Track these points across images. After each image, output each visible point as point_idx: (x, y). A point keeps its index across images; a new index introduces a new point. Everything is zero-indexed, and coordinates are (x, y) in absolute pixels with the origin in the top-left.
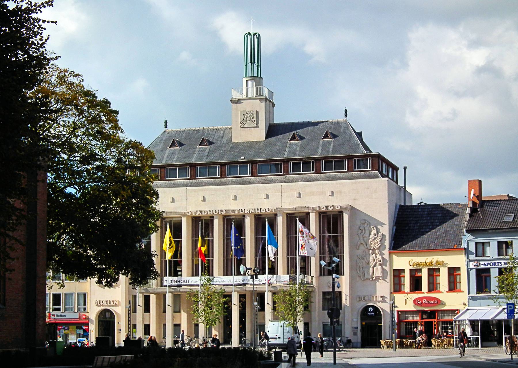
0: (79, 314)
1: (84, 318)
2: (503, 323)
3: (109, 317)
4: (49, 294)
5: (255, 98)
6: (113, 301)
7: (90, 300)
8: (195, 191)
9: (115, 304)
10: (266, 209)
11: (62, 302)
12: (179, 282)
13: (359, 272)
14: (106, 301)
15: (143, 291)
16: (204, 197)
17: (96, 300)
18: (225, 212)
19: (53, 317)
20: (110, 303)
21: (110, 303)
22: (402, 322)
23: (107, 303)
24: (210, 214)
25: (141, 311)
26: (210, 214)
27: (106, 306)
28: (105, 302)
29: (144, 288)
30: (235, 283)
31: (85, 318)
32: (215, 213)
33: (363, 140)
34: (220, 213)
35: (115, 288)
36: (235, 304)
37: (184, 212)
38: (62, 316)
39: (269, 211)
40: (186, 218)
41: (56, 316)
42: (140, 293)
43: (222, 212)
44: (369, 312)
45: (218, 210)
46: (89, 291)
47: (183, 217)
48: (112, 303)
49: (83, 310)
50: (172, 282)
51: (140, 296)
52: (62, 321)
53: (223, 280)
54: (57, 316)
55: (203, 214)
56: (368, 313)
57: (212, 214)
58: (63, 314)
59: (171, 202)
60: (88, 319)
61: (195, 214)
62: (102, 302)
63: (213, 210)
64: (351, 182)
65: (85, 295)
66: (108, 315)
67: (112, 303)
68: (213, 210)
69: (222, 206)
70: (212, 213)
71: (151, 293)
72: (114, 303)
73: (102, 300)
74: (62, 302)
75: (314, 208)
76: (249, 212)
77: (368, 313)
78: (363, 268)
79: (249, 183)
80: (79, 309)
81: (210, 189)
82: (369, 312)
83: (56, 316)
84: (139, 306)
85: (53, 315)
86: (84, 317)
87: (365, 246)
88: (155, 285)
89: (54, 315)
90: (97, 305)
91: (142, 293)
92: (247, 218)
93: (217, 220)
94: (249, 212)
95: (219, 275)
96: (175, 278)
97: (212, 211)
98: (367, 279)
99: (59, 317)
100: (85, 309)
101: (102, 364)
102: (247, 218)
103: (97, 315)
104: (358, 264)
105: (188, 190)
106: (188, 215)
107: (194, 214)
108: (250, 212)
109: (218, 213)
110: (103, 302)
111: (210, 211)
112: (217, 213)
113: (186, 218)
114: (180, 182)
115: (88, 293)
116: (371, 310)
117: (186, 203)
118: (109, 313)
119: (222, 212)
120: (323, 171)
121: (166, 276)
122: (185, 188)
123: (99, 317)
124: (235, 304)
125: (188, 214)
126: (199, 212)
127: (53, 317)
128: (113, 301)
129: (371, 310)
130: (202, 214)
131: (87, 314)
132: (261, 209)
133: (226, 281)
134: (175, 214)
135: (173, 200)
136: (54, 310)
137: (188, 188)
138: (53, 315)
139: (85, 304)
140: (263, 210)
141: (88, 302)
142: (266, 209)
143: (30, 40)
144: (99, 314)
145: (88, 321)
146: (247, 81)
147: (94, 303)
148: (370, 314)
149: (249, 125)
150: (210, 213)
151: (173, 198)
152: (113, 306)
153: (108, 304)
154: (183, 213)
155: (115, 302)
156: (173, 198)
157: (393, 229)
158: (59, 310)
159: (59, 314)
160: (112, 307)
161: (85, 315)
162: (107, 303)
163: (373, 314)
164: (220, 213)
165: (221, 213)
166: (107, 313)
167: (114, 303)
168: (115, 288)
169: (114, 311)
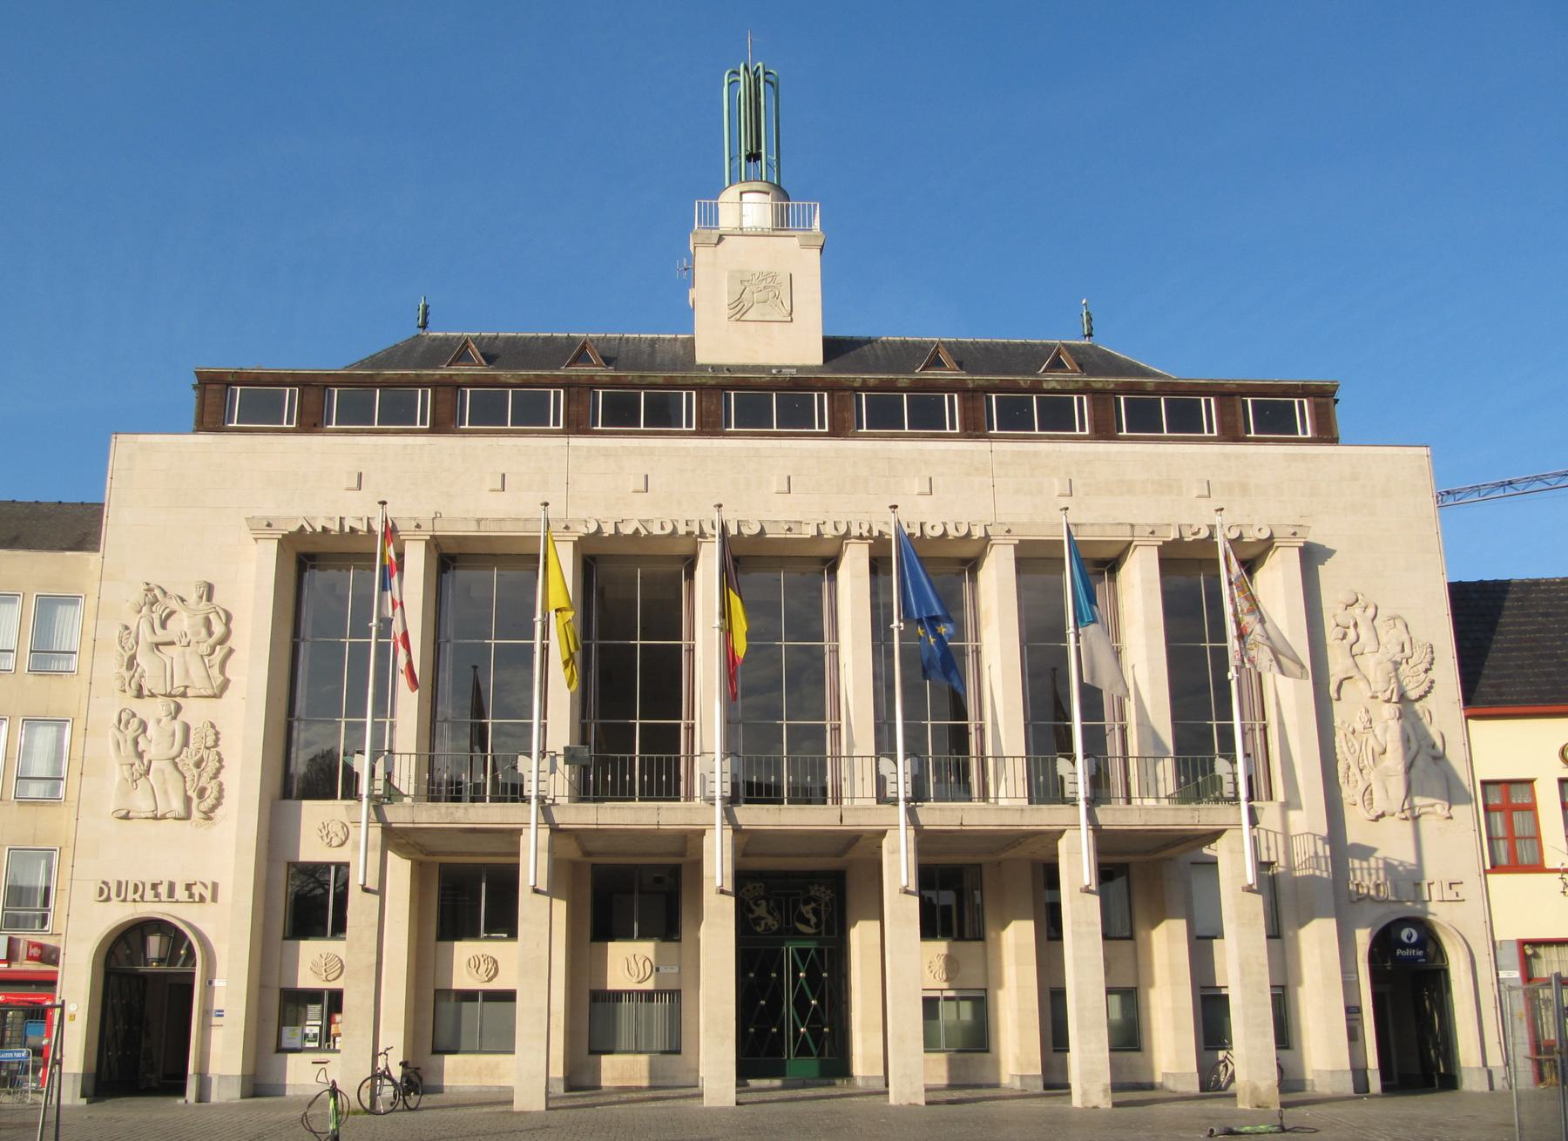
2: (484, 885)
5: (771, 233)
6: (188, 887)
10: (944, 524)
14: (154, 886)
20: (171, 893)
21: (171, 893)
22: (1087, 886)
28: (148, 887)
30: (436, 757)
33: (1265, 537)
44: (1404, 946)
56: (1399, 952)
62: (131, 889)
76: (870, 530)
82: (1404, 946)
94: (870, 530)
101: (417, 1105)
105: (576, 448)
110: (136, 891)
116: (1409, 938)
129: (1409, 938)
142: (944, 524)
143: (1400, 954)
144: (115, 936)
146: (741, 193)
148: (1407, 953)
149: (762, 314)
157: (1395, 860)
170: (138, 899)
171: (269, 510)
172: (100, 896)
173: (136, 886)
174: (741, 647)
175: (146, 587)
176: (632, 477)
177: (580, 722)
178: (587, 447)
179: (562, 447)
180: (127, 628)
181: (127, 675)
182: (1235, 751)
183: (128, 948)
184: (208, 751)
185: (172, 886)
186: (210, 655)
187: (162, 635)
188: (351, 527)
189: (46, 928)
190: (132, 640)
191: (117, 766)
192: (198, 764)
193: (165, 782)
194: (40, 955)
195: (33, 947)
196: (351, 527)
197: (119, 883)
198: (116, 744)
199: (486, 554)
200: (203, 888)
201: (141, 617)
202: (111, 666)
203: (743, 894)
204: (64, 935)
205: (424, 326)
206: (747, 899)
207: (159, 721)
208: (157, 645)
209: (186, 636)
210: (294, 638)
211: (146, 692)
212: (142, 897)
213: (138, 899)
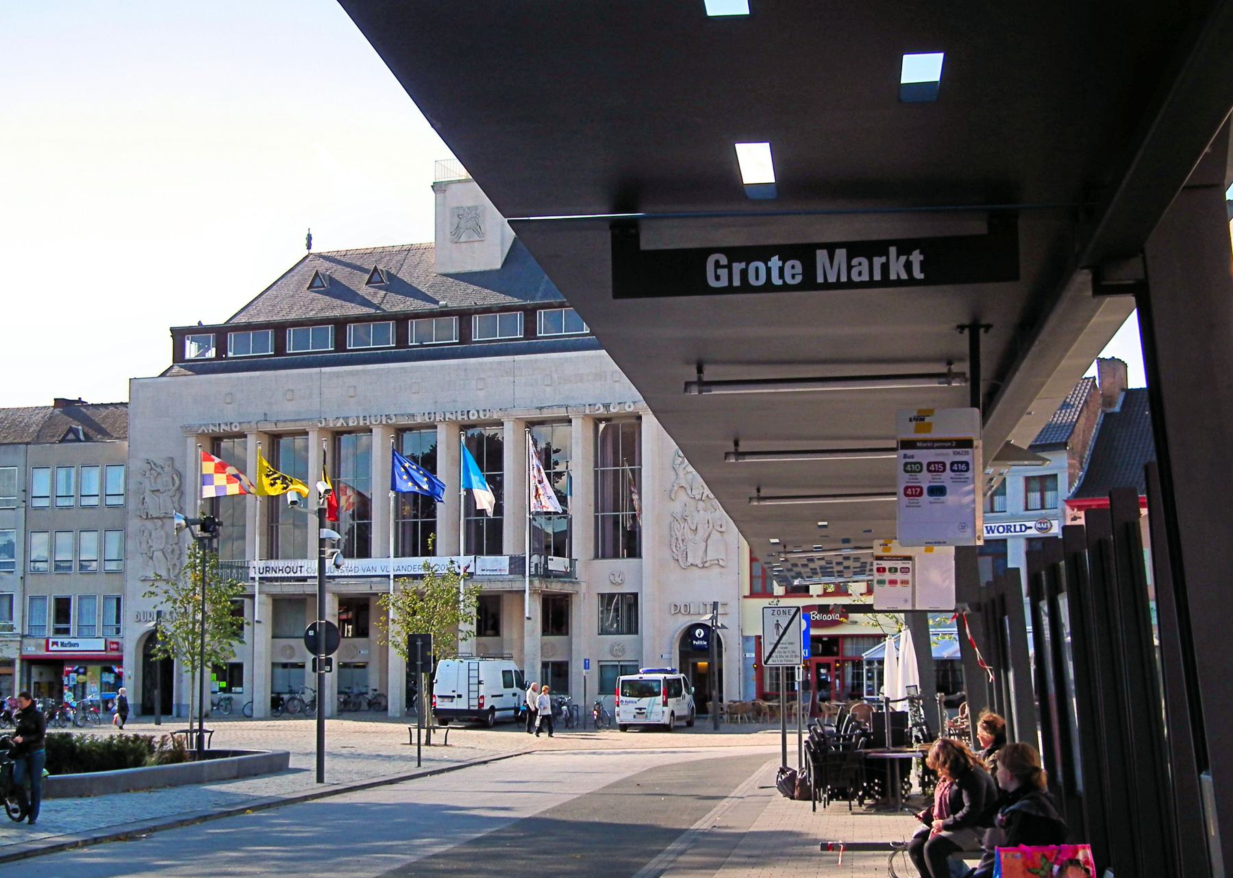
0: (106, 641)
13: (674, 550)
19: (55, 648)
34: (384, 422)
41: (60, 644)
54: (63, 644)
56: (694, 642)
58: (73, 641)
77: (694, 642)
78: (683, 540)
82: (697, 639)
83: (60, 644)
87: (689, 492)
98: (692, 564)
99: (66, 646)
104: (673, 533)
108: (447, 419)
127: (55, 648)
130: (348, 424)
136: (58, 631)
138: (54, 643)
158: (67, 631)
159: (66, 641)
163: (705, 643)
205: (309, 247)
208: (153, 491)
211: (149, 516)
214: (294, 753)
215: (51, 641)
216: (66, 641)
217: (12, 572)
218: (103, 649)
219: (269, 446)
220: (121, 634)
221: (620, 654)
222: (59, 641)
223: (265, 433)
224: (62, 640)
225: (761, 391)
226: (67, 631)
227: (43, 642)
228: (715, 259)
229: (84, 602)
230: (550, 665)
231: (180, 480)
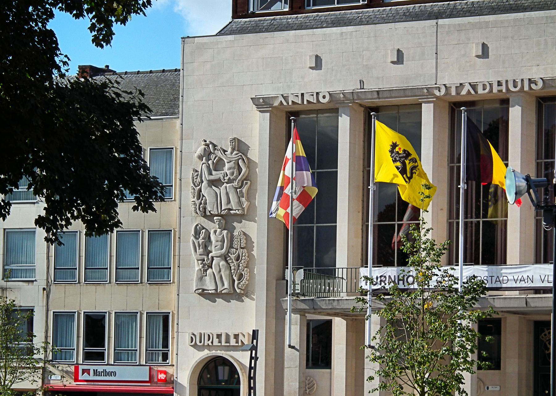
0: (150, 369)
1: (161, 380)
3: (226, 378)
4: (76, 315)
6: (236, 336)
7: (178, 332)
8: (460, 29)
9: (240, 344)
11: (109, 337)
12: (530, 281)
15: (303, 306)
16: (484, 46)
17: (191, 331)
18: (540, 84)
19: (86, 377)
20: (228, 341)
21: (228, 341)
23: (220, 342)
24: (500, 91)
25: (297, 363)
26: (500, 91)
27: (221, 347)
28: (215, 337)
29: (307, 298)
31: (165, 381)
32: (512, 88)
34: (526, 88)
35: (243, 301)
36: (293, 347)
37: (428, 89)
38: (106, 373)
39: (515, 87)
40: (432, 105)
41: (92, 372)
42: (295, 311)
43: (533, 86)
45: (522, 80)
46: (176, 309)
47: (425, 102)
48: (233, 342)
49: (160, 358)
50: (381, 281)
51: (293, 321)
52: (108, 388)
53: (525, 277)
54: (96, 373)
55: (480, 91)
57: (504, 91)
58: (109, 369)
59: (393, 62)
60: (172, 382)
61: (458, 93)
63: (507, 81)
64: (515, 20)
65: (166, 318)
66: (223, 373)
67: (233, 342)
68: (507, 81)
69: (535, 69)
70: (504, 89)
71: (336, 315)
72: (237, 342)
73: (208, 332)
74: (109, 337)
75: (267, 100)
79: (361, 23)
80: (150, 356)
81: (502, 22)
83: (92, 372)
84: (290, 346)
85: (84, 371)
86: (162, 376)
88: (344, 290)
89: (88, 371)
90: (195, 346)
91: (302, 312)
92: (341, 116)
93: (520, 108)
95: (523, 262)
96: (391, 272)
97: (504, 84)
99: (100, 375)
100: (165, 357)
102: (341, 116)
103: (193, 372)
105: (443, 26)
106: (437, 97)
107: (453, 93)
108: (305, 102)
109: (523, 86)
111: (499, 84)
112: (487, 91)
113: (432, 105)
114: (422, 8)
115: (173, 314)
117: (434, 64)
118: (227, 368)
119: (533, 86)
120: (309, 8)
121: (367, 263)
122: (433, 22)
123: (200, 377)
124: (293, 347)
125: (437, 93)
126: (467, 87)
127: (86, 377)
128: (236, 336)
130: (476, 92)
131: (170, 370)
132: (318, 94)
133: (537, 277)
134: (402, 93)
135: (400, 59)
136: (88, 356)
137: (441, 21)
138: (84, 371)
139: (166, 344)
140: (324, 97)
141: (173, 338)
145: (173, 388)
147: (188, 340)
150: (500, 88)
151: (399, 51)
152: (235, 348)
153: (223, 344)
154: (425, 91)
155: (241, 337)
156: (399, 51)
158: (100, 356)
159: (100, 369)
160: (232, 353)
161: (165, 373)
162: (220, 342)
164: (526, 88)
165: (530, 88)
166: (220, 368)
167: (237, 342)
168: (243, 301)
169: (237, 361)
170: (210, 344)
171: (267, 91)
172: (192, 342)
173: (209, 335)
174: (294, 151)
175: (204, 143)
176: (474, 45)
177: (447, 221)
178: (448, 25)
179: (433, 26)
180: (197, 171)
181: (198, 202)
182: (335, 164)
183: (209, 374)
184: (242, 250)
185: (228, 336)
186: (240, 187)
187: (216, 175)
188: (292, 101)
189: (168, 362)
190: (199, 179)
191: (196, 261)
192: (238, 259)
193: (220, 271)
194: (165, 378)
195: (161, 374)
196: (292, 101)
197: (201, 334)
198: (220, 277)
199: (386, 106)
200: (243, 337)
201: (203, 164)
202: (189, 198)
203: (543, 337)
204: (175, 366)
206: (545, 340)
207: (215, 232)
209: (227, 175)
210: (537, 216)
212: (212, 343)
213: (210, 344)
214: (331, 371)
215: (81, 368)
216: (100, 369)
217: (33, 281)
218: (148, 380)
219: (365, 123)
220: (169, 361)
221: (197, 173)
222: (92, 368)
223: (361, 105)
224: (95, 368)
225: (543, 155)
226: (100, 356)
227: (72, 369)
228: (539, 84)
229: (438, 88)
230: (315, 223)
231: (248, 167)
